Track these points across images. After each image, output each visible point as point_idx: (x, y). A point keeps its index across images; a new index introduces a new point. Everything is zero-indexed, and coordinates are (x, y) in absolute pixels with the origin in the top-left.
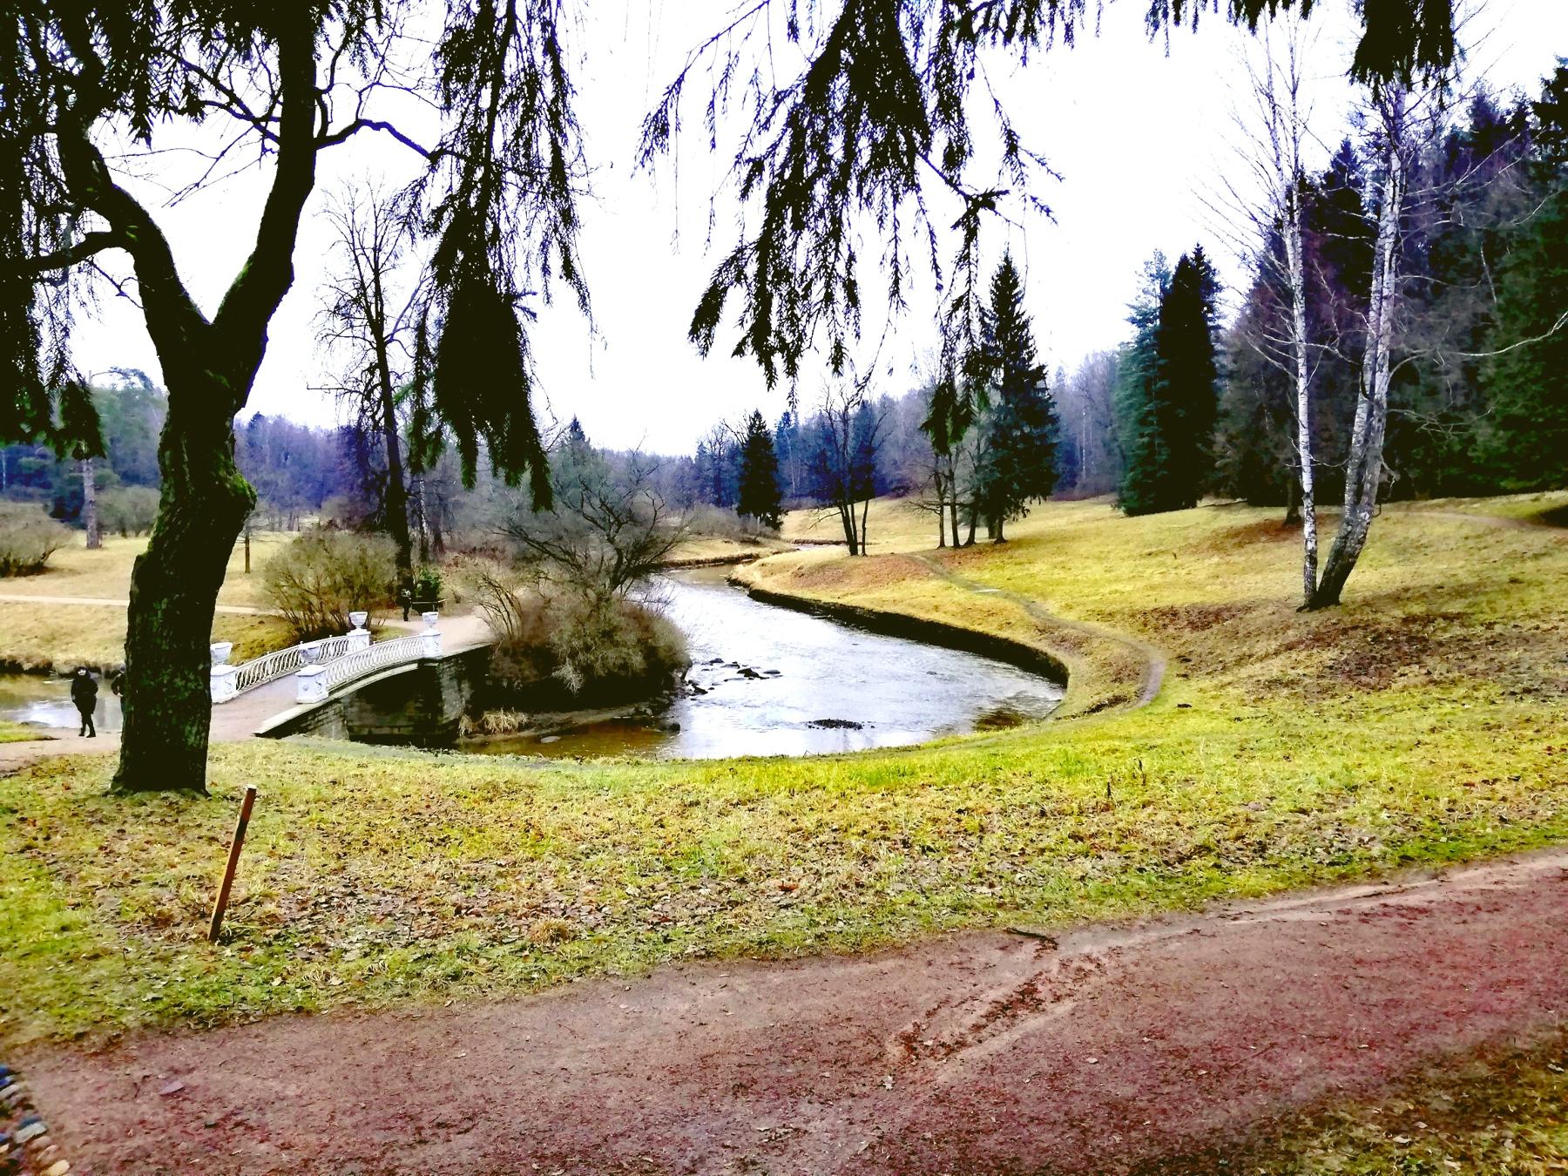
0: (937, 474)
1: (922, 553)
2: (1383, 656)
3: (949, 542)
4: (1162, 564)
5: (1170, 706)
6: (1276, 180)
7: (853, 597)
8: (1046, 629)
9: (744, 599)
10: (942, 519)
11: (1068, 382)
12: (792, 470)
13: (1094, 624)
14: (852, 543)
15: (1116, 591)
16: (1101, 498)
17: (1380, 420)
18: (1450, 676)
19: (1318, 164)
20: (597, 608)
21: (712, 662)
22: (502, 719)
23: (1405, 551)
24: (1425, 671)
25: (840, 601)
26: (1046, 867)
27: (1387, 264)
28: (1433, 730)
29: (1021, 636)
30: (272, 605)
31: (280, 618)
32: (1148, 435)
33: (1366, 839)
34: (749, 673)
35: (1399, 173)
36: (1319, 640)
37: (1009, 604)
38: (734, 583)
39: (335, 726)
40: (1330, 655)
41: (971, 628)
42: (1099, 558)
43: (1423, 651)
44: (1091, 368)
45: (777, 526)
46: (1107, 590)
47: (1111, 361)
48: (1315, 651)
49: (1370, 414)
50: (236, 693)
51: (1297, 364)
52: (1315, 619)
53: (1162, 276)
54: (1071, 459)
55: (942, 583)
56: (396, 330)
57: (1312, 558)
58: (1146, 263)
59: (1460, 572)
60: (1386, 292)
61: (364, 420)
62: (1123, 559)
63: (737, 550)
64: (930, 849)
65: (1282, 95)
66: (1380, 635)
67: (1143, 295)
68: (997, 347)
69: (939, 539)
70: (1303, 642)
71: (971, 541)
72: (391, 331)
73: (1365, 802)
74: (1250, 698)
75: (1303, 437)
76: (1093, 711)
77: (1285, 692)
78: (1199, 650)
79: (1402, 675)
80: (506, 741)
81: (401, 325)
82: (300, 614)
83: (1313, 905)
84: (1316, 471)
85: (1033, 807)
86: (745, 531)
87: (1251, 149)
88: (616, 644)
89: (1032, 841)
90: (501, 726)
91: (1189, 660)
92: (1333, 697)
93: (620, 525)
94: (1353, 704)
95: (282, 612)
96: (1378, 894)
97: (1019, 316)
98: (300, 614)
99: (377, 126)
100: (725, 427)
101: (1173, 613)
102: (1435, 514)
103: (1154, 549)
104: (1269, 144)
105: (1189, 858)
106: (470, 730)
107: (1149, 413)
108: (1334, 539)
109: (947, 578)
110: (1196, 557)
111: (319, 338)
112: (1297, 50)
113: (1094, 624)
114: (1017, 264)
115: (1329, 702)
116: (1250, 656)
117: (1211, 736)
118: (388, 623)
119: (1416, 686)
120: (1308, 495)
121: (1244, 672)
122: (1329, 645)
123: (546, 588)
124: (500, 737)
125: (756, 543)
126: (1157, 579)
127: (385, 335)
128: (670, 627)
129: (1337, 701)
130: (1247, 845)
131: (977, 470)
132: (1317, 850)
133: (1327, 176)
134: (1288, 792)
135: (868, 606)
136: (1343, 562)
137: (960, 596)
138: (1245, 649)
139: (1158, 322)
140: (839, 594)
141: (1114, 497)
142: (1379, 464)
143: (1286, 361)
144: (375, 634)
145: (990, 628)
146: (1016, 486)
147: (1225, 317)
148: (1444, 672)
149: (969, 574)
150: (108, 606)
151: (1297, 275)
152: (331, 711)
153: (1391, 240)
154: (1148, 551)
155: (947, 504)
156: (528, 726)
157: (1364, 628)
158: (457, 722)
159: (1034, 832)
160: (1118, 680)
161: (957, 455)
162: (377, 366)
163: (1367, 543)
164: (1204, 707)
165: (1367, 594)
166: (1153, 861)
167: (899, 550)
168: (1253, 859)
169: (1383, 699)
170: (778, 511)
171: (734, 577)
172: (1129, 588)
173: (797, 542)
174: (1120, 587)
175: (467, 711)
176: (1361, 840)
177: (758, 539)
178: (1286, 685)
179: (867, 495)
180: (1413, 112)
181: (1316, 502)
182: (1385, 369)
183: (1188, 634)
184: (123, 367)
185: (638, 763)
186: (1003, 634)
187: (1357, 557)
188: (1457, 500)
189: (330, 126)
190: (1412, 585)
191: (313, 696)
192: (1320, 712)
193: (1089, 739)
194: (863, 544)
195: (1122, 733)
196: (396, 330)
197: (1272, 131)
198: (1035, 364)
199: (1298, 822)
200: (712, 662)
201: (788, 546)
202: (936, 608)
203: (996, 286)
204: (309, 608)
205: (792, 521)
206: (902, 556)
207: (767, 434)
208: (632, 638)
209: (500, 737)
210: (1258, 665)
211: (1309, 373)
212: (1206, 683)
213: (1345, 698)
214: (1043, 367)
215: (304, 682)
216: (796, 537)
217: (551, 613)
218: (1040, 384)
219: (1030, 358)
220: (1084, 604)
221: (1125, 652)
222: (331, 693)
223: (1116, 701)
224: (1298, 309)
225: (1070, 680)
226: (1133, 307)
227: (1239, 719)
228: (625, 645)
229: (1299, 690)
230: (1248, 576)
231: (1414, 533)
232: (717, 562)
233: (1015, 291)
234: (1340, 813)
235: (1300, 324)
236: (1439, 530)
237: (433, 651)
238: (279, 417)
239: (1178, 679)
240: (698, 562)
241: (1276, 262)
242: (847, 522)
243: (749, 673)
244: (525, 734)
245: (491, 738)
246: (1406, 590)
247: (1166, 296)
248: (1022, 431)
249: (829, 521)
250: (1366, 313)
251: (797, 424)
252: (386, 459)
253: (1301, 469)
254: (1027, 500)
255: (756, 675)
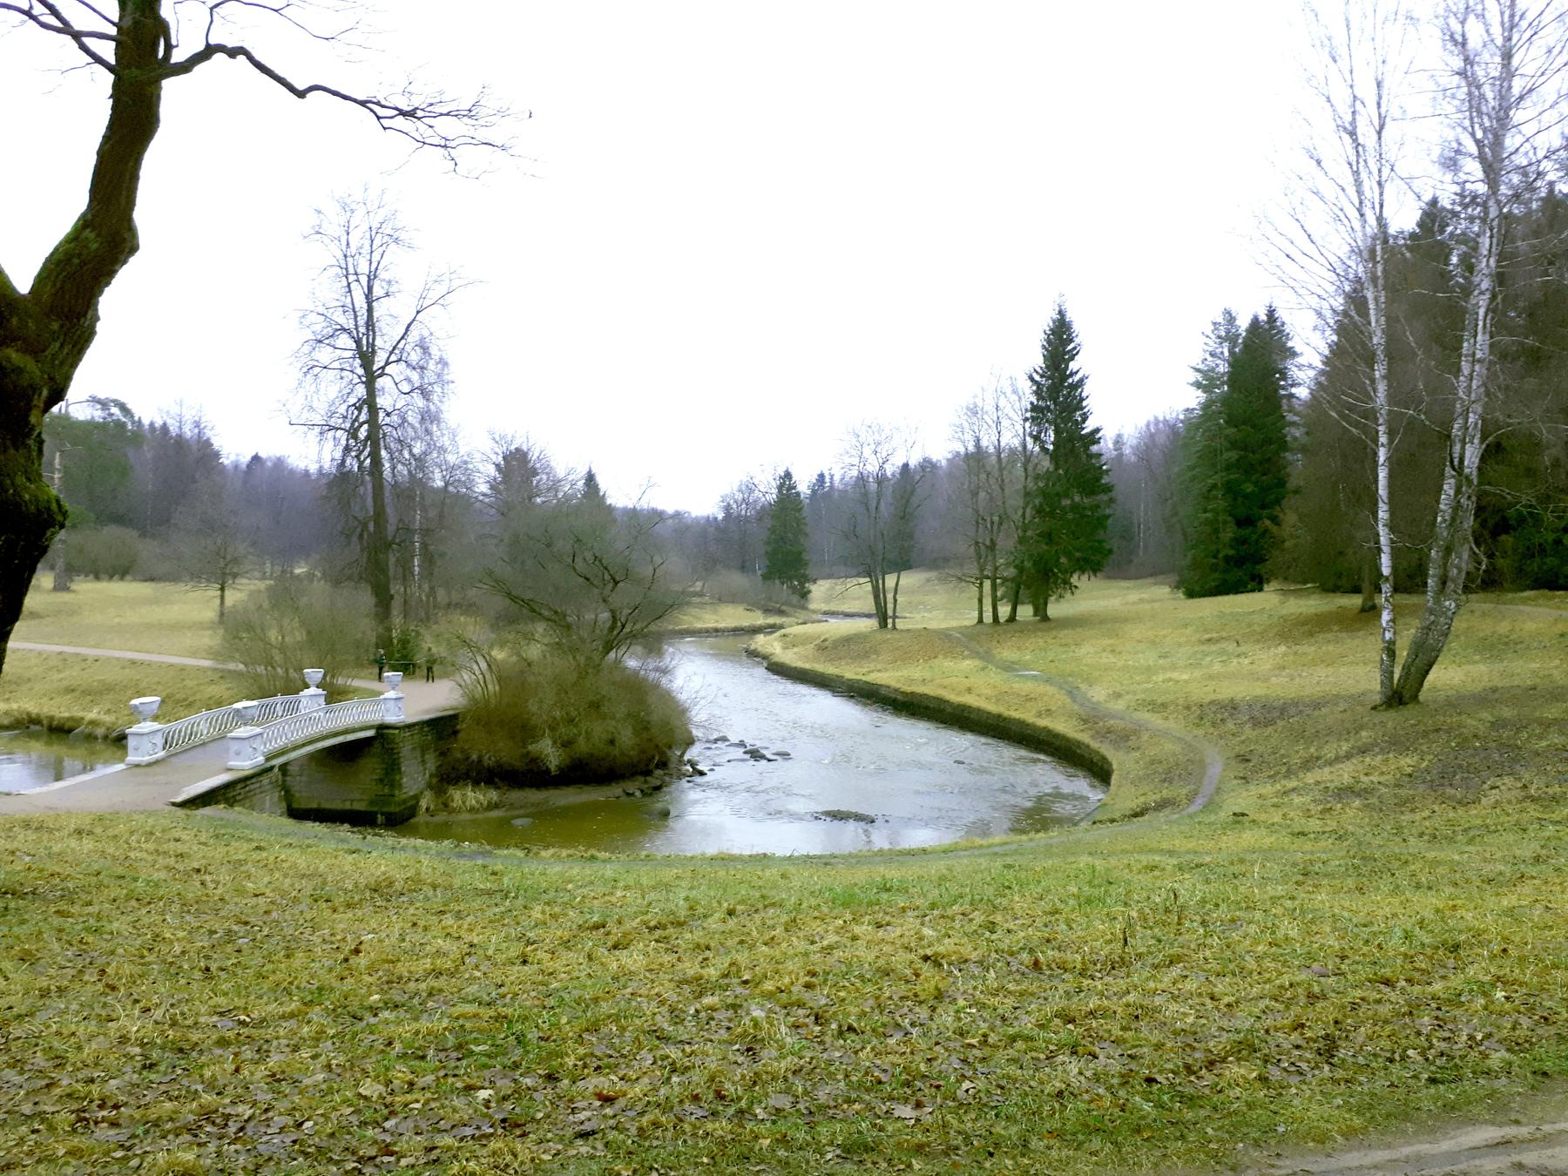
0: (977, 543)
1: (960, 629)
2: (1469, 765)
3: (988, 617)
4: (1223, 652)
5: (1224, 815)
6: (1357, 225)
7: (879, 675)
8: (1091, 718)
9: (761, 672)
10: (981, 592)
11: (1127, 451)
12: (822, 540)
13: (1144, 716)
14: (882, 616)
15: (1170, 679)
16: (1160, 578)
17: (1469, 498)
18: (1550, 791)
19: (1404, 219)
20: (582, 675)
21: (716, 741)
22: (468, 797)
23: (1493, 648)
24: (1520, 785)
25: (864, 678)
26: (1013, 1070)
27: (1481, 323)
28: (1537, 859)
29: (1063, 726)
30: (232, 658)
31: (239, 674)
32: (1211, 510)
33: (1479, 1037)
34: (756, 755)
35: (1495, 223)
36: (1398, 744)
37: (1051, 690)
38: (752, 654)
39: (272, 798)
40: (1408, 760)
41: (1006, 713)
42: (1153, 643)
43: (1515, 760)
44: (1152, 436)
45: (805, 595)
46: (1161, 678)
47: (1172, 428)
48: (1391, 755)
49: (1458, 491)
50: (162, 754)
51: (1377, 432)
52: (1392, 718)
53: (1231, 338)
54: (1127, 535)
55: (977, 663)
56: (387, 363)
57: (1391, 651)
58: (1215, 324)
59: (1555, 672)
60: (1479, 355)
61: (348, 462)
62: (1180, 645)
63: (759, 619)
64: (851, 1029)
65: (1367, 135)
66: (1466, 739)
67: (1210, 358)
68: (1048, 407)
69: (976, 614)
70: (1378, 745)
71: (1012, 618)
72: (382, 364)
73: (1471, 971)
74: (1316, 809)
75: (1383, 514)
76: (1136, 815)
77: (1357, 803)
78: (1261, 749)
79: (1493, 788)
80: (473, 821)
81: (393, 358)
82: (261, 669)
83: (1407, 1160)
84: (1396, 554)
85: (1025, 956)
86: (770, 599)
87: (1329, 191)
88: (604, 717)
89: (1004, 1019)
90: (468, 804)
91: (1248, 761)
92: (1412, 811)
93: (616, 583)
94: (1437, 822)
95: (241, 667)
96: (1506, 1143)
97: (1072, 374)
98: (261, 669)
99: (233, 53)
100: (750, 488)
101: (1232, 707)
102: (1527, 609)
103: (1215, 635)
104: (1351, 191)
105: (1224, 1060)
106: (432, 807)
107: (1214, 486)
108: (1413, 631)
109: (982, 658)
110: (1261, 646)
111: (305, 370)
112: (1386, 85)
113: (1144, 716)
114: (1070, 316)
115: (1407, 817)
116: (1318, 758)
117: (1268, 854)
118: (357, 683)
119: (1509, 802)
120: (1387, 579)
121: (1310, 778)
122: (1408, 749)
123: (534, 651)
124: (466, 816)
125: (781, 613)
126: (1217, 667)
127: (375, 368)
128: (667, 698)
129: (1418, 817)
130: (1308, 1040)
131: (1021, 540)
132: (1410, 1052)
133: (1413, 236)
134: (1365, 949)
135: (894, 684)
136: (1424, 658)
137: (995, 678)
138: (1312, 750)
139: (1226, 388)
140: (865, 670)
141: (1174, 578)
142: (1467, 546)
143: (1364, 428)
144: (334, 694)
145: (1027, 715)
146: (1063, 560)
147: (1300, 384)
148: (1542, 785)
149: (1007, 653)
150: (60, 653)
151: (1379, 333)
152: (265, 780)
153: (1488, 296)
154: (1207, 636)
155: (988, 578)
156: (496, 806)
157: (1448, 732)
158: (417, 798)
159: (1010, 1002)
160: (1167, 779)
161: (1001, 524)
162: (365, 402)
163: (1451, 637)
164: (1263, 817)
165: (1449, 693)
166: (1170, 1066)
167: (933, 625)
168: (1317, 1067)
169: (1473, 816)
170: (805, 579)
171: (752, 647)
172: (1185, 677)
173: (826, 613)
174: (1175, 675)
175: (430, 786)
176: (1471, 1037)
177: (784, 608)
178: (1359, 795)
179: (903, 564)
180: (1513, 157)
181: (1396, 590)
182: (1476, 441)
183: (1248, 731)
184: (102, 396)
185: (593, 857)
186: (1043, 722)
187: (1439, 651)
188: (1550, 593)
189: (175, 51)
190: (1500, 685)
191: (246, 762)
192: (1399, 830)
193: (1124, 852)
194: (894, 617)
195: (1165, 846)
196: (387, 363)
197: (1356, 173)
198: (1089, 426)
199: (1379, 1001)
200: (716, 741)
201: (815, 617)
202: (969, 690)
203: (1049, 341)
204: (270, 663)
205: (819, 590)
206: (935, 631)
207: (798, 494)
208: (621, 711)
209: (466, 816)
210: (1327, 770)
211: (1391, 441)
212: (1268, 789)
213: (1427, 813)
214: (1097, 430)
215: (234, 746)
216: (824, 607)
217: (531, 679)
218: (1094, 448)
219: (1084, 420)
220: (1135, 693)
221: (1177, 748)
222: (267, 760)
223: (1161, 805)
224: (1380, 370)
225: (1114, 779)
226: (1198, 370)
227: (1303, 834)
228: (614, 718)
229: (1374, 800)
230: (1318, 669)
231: (1503, 627)
232: (737, 631)
233: (1069, 348)
234: (1438, 987)
235: (1382, 387)
236: (1530, 626)
237: (393, 716)
238: (279, 459)
239: (1235, 782)
240: (716, 630)
241: (1356, 317)
242: (878, 594)
243: (756, 755)
244: (495, 814)
245: (454, 818)
246: (1494, 690)
247: (1234, 362)
248: (1073, 500)
249: (859, 593)
250: (1457, 377)
251: (832, 486)
252: (370, 502)
253: (1379, 550)
254: (1075, 576)
255: (763, 757)
